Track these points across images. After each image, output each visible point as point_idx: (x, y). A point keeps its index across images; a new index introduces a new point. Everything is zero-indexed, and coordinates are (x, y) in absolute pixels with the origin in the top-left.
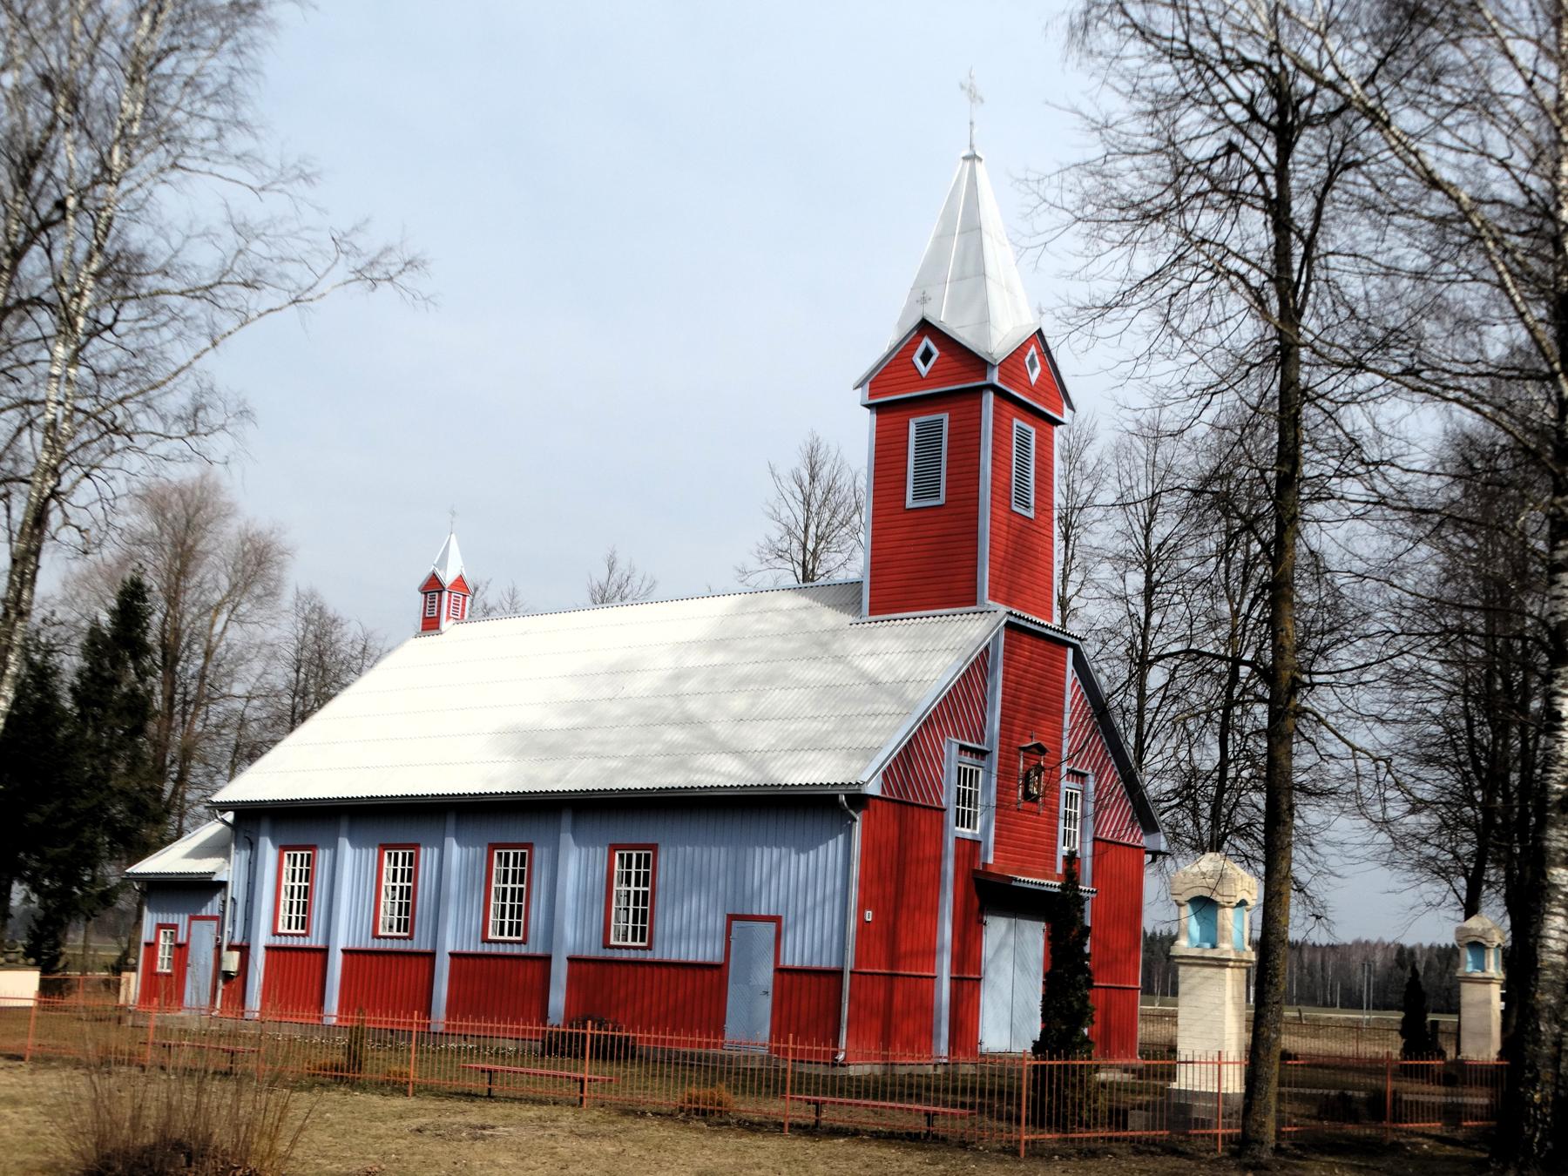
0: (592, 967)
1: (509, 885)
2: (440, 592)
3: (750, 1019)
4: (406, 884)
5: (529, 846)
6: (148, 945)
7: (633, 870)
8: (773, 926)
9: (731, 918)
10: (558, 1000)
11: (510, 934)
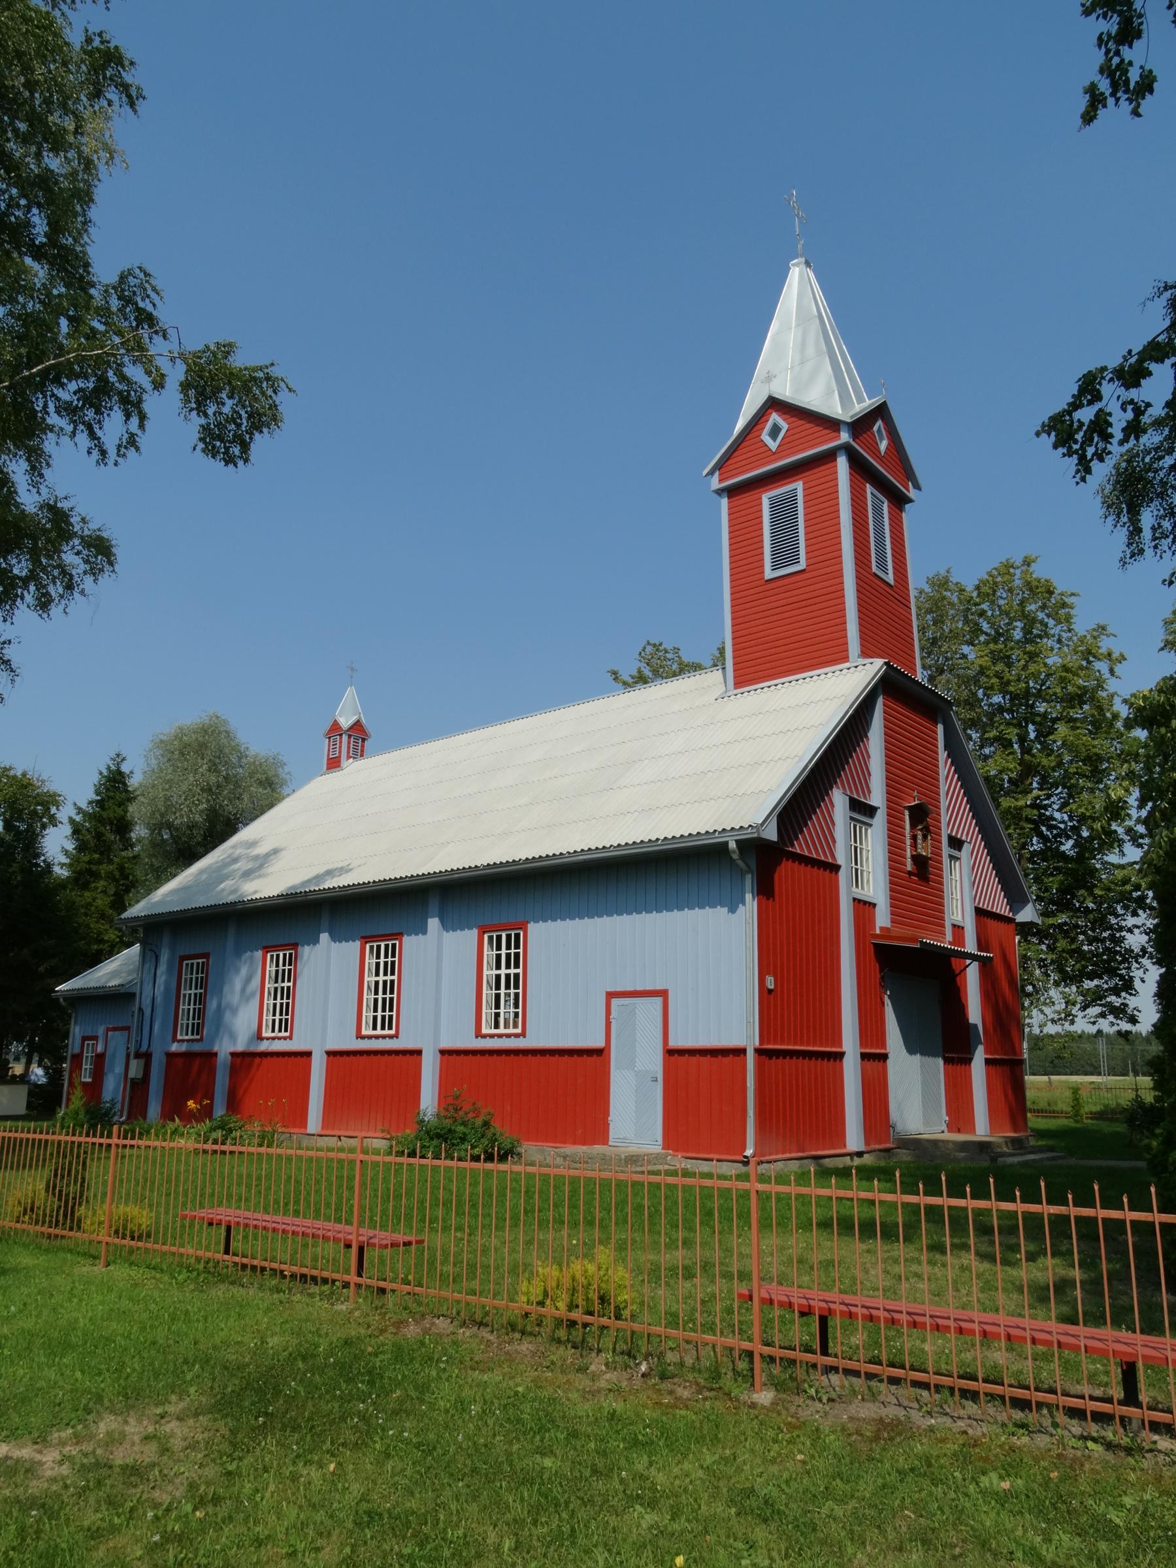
0: (706, 1060)
1: (381, 978)
2: (341, 735)
3: (635, 1116)
4: (199, 991)
5: (206, 956)
6: (74, 1056)
7: (382, 960)
8: (659, 1000)
9: (611, 995)
10: (428, 1100)
11: (383, 1028)
